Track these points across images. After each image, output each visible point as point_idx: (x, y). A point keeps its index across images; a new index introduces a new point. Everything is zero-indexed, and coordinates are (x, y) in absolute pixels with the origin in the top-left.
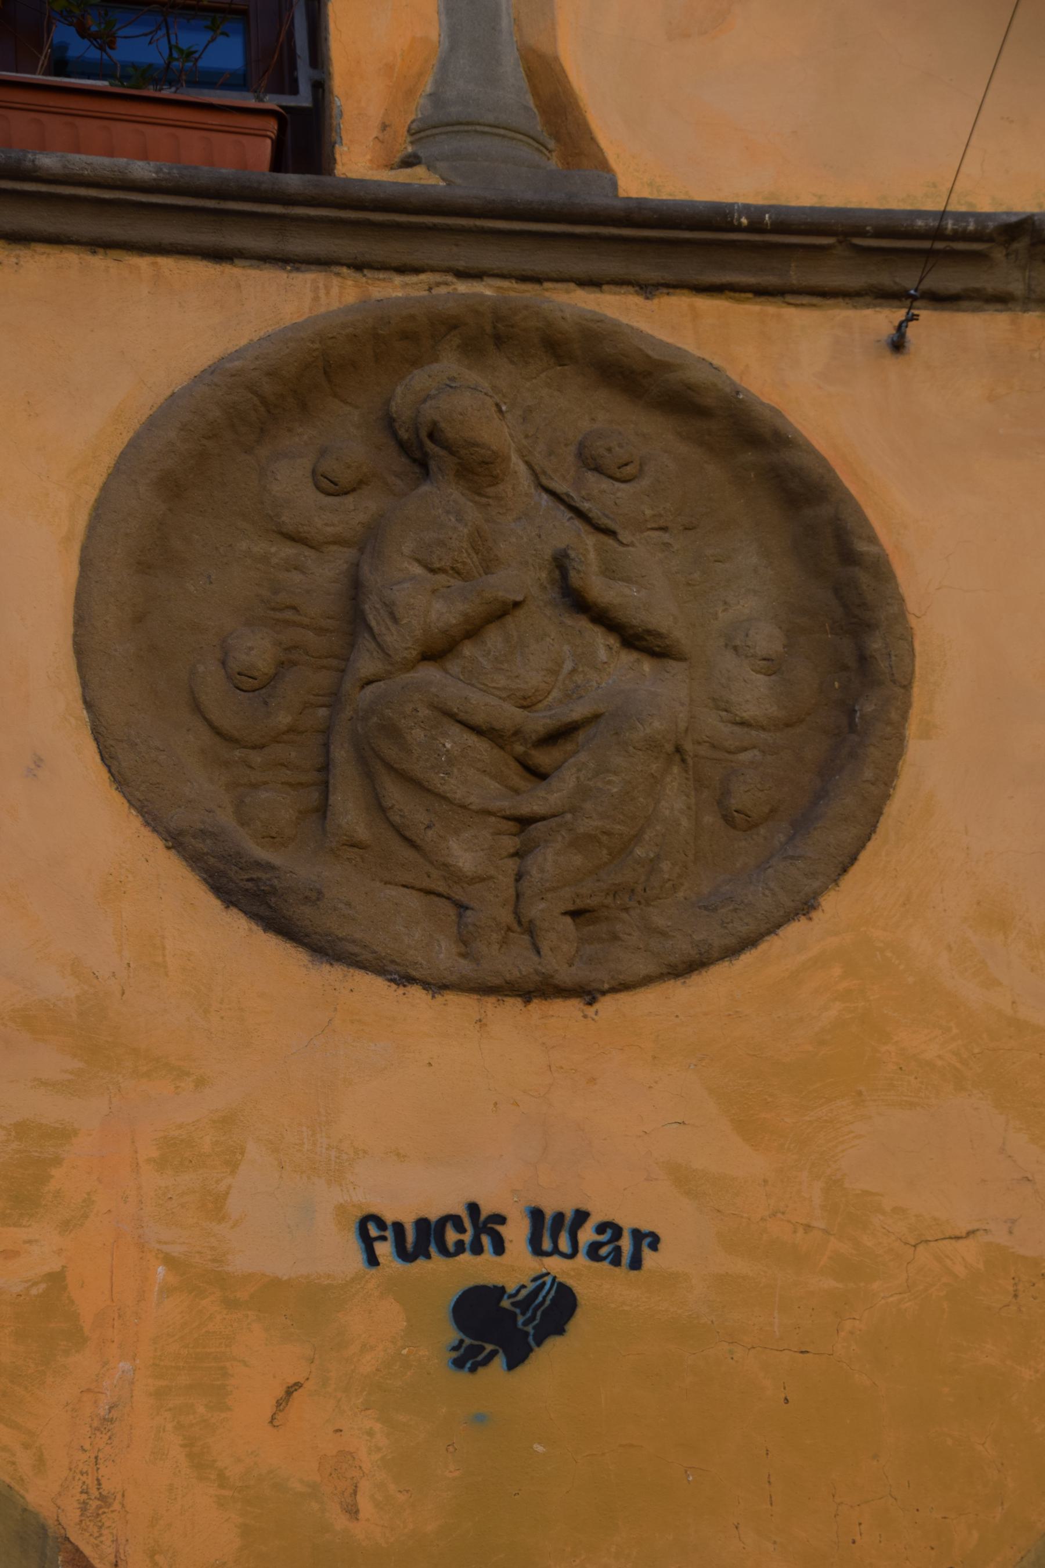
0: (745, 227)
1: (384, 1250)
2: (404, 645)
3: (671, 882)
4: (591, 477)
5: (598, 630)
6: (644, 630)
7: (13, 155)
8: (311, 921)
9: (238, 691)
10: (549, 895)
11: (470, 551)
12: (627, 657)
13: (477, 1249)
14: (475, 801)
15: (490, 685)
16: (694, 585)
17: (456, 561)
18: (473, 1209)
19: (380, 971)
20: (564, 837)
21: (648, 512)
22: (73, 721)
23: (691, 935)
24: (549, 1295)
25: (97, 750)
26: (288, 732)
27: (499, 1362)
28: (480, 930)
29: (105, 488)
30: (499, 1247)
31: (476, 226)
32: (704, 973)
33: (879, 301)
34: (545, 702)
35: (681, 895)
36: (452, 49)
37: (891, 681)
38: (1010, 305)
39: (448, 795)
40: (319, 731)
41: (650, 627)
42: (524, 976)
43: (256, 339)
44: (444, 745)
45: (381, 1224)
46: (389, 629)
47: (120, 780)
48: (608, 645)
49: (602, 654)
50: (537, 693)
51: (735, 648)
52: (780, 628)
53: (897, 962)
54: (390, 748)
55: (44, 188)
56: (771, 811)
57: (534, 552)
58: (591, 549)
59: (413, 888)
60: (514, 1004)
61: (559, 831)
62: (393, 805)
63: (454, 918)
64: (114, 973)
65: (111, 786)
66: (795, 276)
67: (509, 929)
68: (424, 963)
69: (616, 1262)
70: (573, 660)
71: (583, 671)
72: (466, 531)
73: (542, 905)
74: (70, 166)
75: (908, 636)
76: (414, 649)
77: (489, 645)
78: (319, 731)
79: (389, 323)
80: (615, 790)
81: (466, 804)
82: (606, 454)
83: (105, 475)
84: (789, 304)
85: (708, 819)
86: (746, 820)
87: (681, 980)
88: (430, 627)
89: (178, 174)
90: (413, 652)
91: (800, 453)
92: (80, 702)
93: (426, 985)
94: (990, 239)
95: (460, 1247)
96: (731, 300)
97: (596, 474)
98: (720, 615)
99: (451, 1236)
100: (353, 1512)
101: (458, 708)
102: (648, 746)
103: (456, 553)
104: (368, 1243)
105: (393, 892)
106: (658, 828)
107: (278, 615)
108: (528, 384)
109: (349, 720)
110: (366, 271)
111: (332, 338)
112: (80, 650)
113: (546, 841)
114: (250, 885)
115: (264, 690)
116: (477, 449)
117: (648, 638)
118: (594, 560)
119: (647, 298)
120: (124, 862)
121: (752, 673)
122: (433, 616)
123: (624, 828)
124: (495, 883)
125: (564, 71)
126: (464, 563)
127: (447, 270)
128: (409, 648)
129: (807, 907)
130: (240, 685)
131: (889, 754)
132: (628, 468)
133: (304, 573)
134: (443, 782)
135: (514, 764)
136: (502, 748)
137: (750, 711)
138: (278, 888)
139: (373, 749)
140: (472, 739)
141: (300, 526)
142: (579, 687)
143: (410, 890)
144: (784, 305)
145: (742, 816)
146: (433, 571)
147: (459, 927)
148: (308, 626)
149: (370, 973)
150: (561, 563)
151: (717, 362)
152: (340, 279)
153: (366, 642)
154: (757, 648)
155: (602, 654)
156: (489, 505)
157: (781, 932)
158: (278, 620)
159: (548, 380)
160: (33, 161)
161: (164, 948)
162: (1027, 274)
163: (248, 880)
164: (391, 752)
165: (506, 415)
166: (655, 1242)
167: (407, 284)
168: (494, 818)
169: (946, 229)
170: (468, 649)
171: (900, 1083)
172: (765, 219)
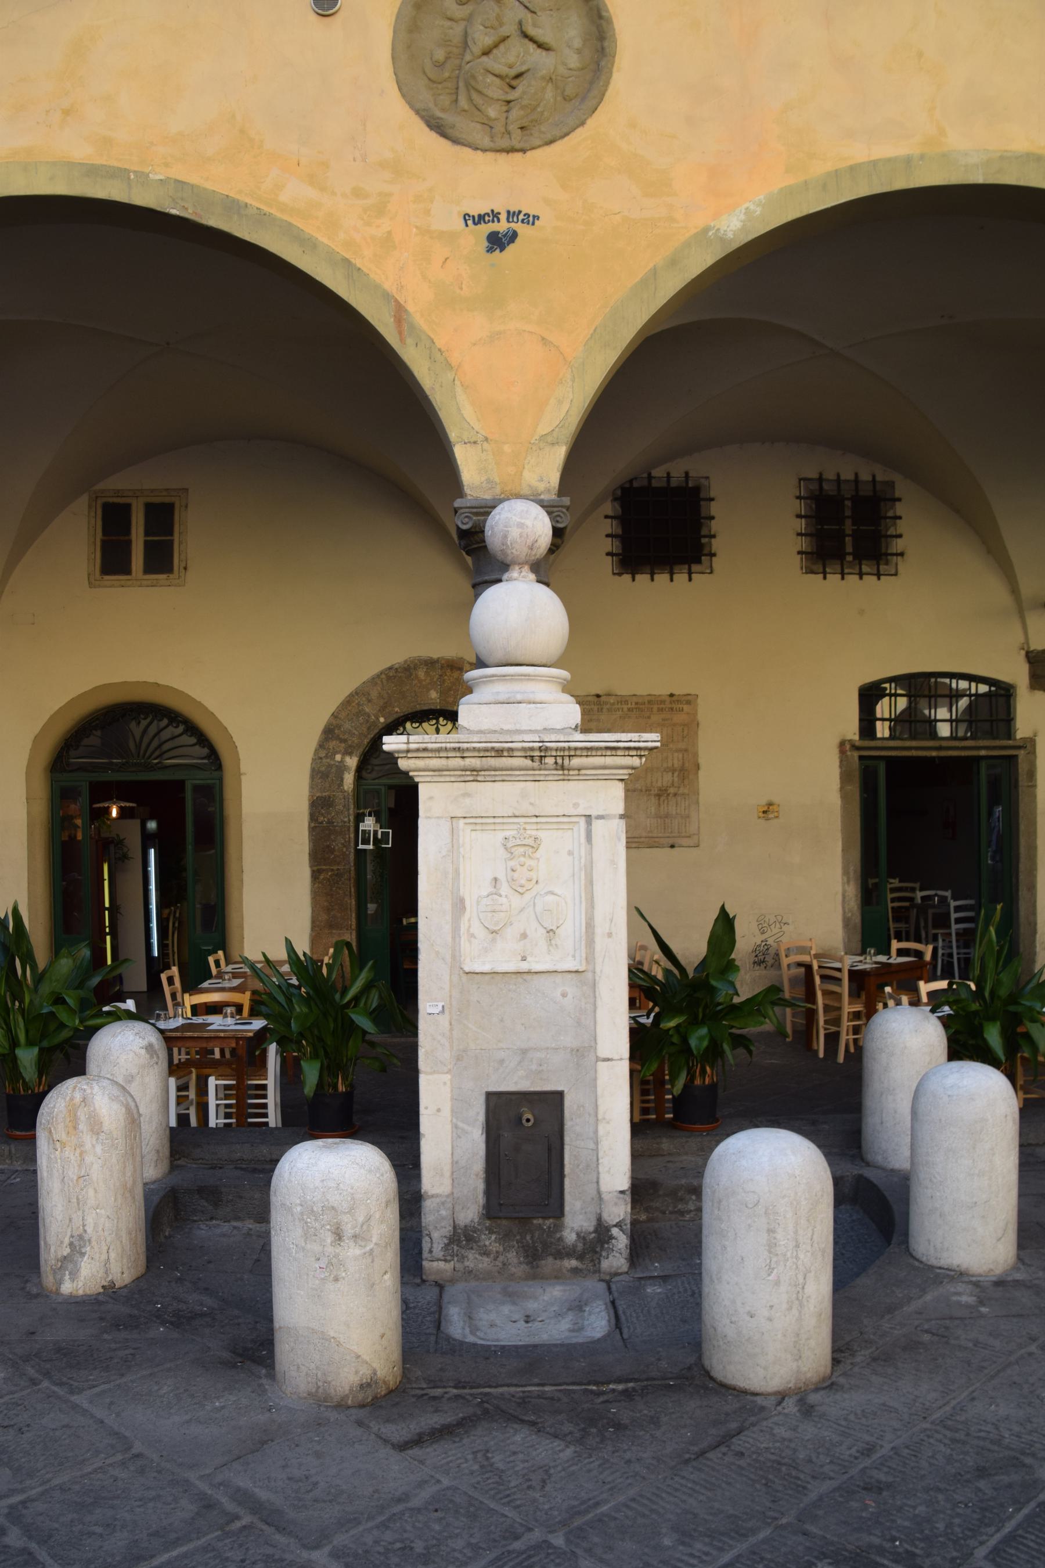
1: (470, 222)
12: (539, 51)
13: (493, 221)
14: (495, 96)
18: (492, 211)
19: (470, 147)
21: (547, 5)
24: (510, 233)
27: (498, 251)
29: (400, 9)
30: (499, 221)
40: (454, 1221)
45: (469, 216)
47: (403, 96)
49: (532, 50)
60: (504, 155)
69: (528, 224)
75: (615, 42)
78: (454, 1221)
85: (559, 98)
95: (489, 221)
99: (487, 218)
100: (461, 289)
104: (466, 221)
105: (473, 124)
112: (393, 58)
129: (583, 123)
137: (572, 66)
140: (495, 78)
146: (486, 27)
150: (520, 23)
153: (468, 51)
155: (532, 50)
164: (473, 83)
166: (538, 218)
170: (495, 51)
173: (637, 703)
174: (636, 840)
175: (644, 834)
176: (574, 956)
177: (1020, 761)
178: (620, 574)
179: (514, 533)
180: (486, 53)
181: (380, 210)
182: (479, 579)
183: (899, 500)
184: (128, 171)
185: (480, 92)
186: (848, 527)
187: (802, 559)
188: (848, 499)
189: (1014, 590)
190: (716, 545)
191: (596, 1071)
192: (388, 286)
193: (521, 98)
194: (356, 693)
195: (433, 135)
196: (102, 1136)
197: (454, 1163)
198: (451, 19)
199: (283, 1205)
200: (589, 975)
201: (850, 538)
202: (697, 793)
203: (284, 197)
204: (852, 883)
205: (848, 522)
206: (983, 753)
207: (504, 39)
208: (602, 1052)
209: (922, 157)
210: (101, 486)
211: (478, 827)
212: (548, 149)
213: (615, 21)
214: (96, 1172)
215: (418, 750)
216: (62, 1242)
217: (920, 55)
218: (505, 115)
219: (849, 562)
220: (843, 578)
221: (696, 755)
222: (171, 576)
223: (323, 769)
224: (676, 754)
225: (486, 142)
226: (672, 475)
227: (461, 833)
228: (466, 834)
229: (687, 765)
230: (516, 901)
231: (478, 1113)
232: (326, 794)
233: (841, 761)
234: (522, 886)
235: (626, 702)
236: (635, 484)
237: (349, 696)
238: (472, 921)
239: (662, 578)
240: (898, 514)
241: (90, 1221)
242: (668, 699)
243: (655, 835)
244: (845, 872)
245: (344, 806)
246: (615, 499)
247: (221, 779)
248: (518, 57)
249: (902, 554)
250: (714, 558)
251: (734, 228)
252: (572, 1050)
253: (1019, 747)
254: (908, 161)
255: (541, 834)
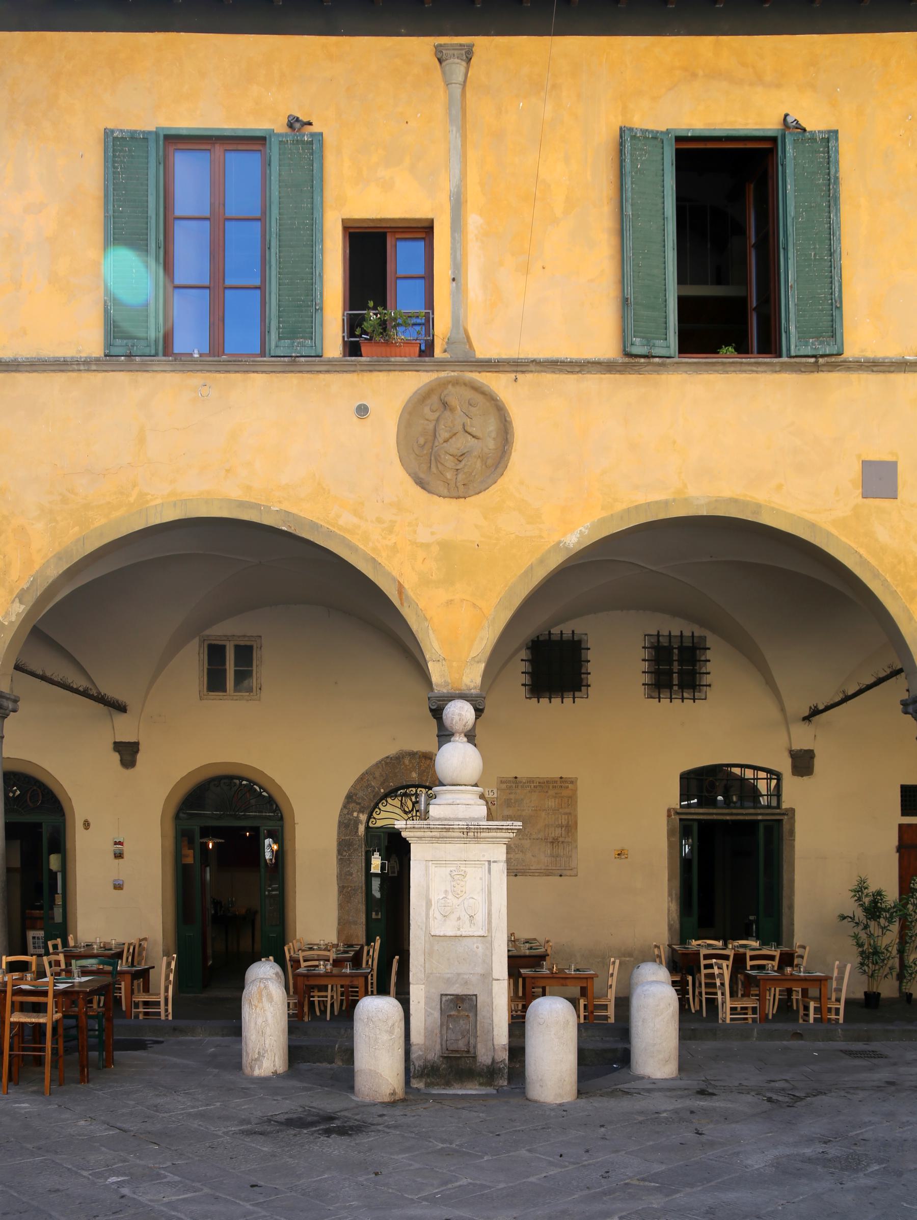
12: (473, 439)
60: (455, 499)
85: (484, 467)
100: (432, 575)
137: (490, 448)
164: (439, 459)
170: (450, 440)
173: (539, 783)
174: (538, 871)
175: (543, 868)
176: (482, 929)
177: (784, 823)
178: (530, 698)
179: (456, 718)
180: (446, 441)
181: (390, 530)
182: (442, 733)
183: (709, 649)
184: (261, 505)
185: (443, 465)
186: (676, 667)
187: (645, 688)
188: (675, 648)
189: (783, 710)
190: (591, 679)
191: (492, 985)
192: (395, 573)
194: (366, 773)
196: (273, 1003)
197: (426, 1029)
198: (427, 420)
199: (360, 1019)
200: (489, 938)
201: (677, 674)
202: (576, 841)
203: (341, 522)
204: (674, 902)
205: (676, 664)
206: (760, 817)
208: (495, 976)
209: (674, 500)
210: (208, 632)
211: (438, 865)
212: (477, 496)
214: (270, 1020)
215: (411, 828)
216: (254, 1052)
217: (674, 442)
219: (675, 690)
220: (671, 702)
221: (576, 816)
222: (252, 694)
223: (346, 821)
224: (563, 816)
225: (446, 492)
226: (563, 632)
227: (430, 868)
228: (432, 869)
229: (570, 823)
230: (455, 901)
231: (437, 1005)
232: (348, 837)
233: (668, 822)
234: (458, 894)
235: (533, 782)
236: (541, 638)
237: (362, 775)
238: (435, 912)
239: (556, 701)
240: (708, 659)
241: (267, 1042)
242: (559, 780)
243: (550, 868)
244: (670, 894)
245: (359, 846)
246: (528, 648)
247: (282, 827)
249: (709, 686)
250: (589, 688)
251: (573, 542)
252: (481, 975)
253: (784, 814)
254: (666, 503)
255: (467, 869)
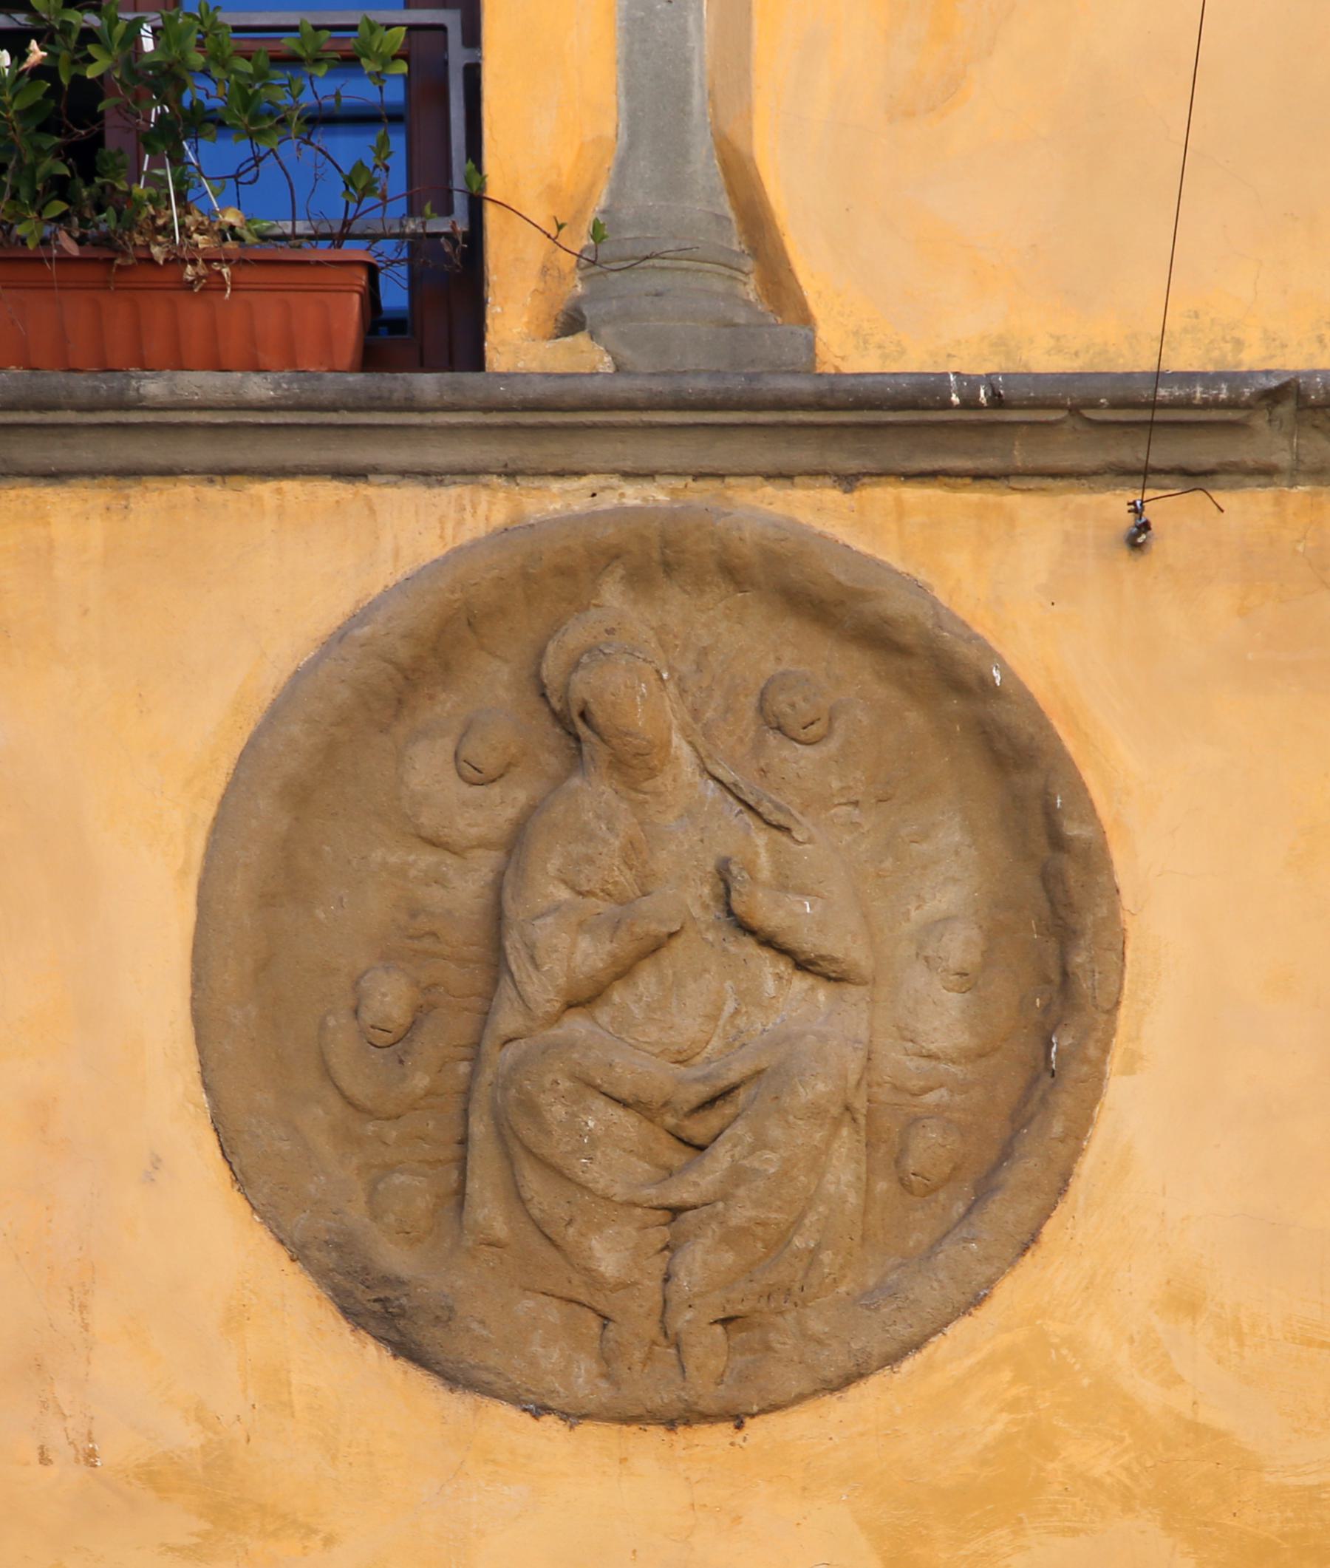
0: (957, 405)
2: (546, 997)
3: (833, 1276)
4: (772, 739)
5: (767, 955)
6: (816, 956)
7: (115, 384)
8: (441, 1347)
9: (372, 1047)
10: (697, 1302)
11: (622, 867)
12: (801, 983)
15: (641, 1039)
16: (885, 877)
17: (607, 881)
19: (515, 1400)
20: (714, 1231)
21: (836, 784)
22: (191, 1108)
23: (849, 1343)
25: (217, 1144)
26: (426, 1096)
28: (621, 1348)
29: (223, 802)
31: (642, 421)
32: (862, 1384)
33: (1121, 479)
34: (704, 1055)
35: (842, 1289)
36: (631, 146)
37: (1094, 1005)
38: (1275, 479)
39: (590, 1185)
41: (823, 952)
42: (666, 1404)
43: (391, 585)
44: (587, 1123)
46: (529, 976)
47: (241, 1180)
48: (777, 974)
49: (770, 986)
50: (693, 1046)
51: (927, 959)
52: (980, 927)
53: (1074, 1360)
54: (529, 1129)
55: (151, 417)
56: (954, 1169)
57: (695, 863)
58: (762, 851)
59: (553, 1296)
60: (656, 1434)
61: (709, 1224)
62: (533, 1197)
63: (596, 1330)
64: (238, 1416)
65: (233, 1187)
66: (1019, 458)
67: (654, 1343)
68: (561, 1390)
70: (736, 1000)
71: (746, 1012)
72: (617, 843)
73: (689, 1315)
74: (178, 392)
76: (557, 1001)
77: (641, 988)
79: (541, 559)
80: (772, 1170)
81: (610, 1196)
82: (788, 710)
83: (224, 785)
84: (1014, 489)
85: (881, 1186)
86: (925, 1184)
87: (838, 1394)
88: (574, 972)
89: (299, 389)
90: (555, 1003)
91: (1009, 706)
92: (199, 1083)
93: (565, 1416)
94: (1248, 406)
96: (945, 488)
97: (779, 735)
98: (913, 914)
101: (602, 1079)
102: (809, 1115)
103: (606, 873)
106: (821, 1209)
107: (416, 945)
108: (704, 618)
109: (490, 1085)
110: (519, 479)
111: (475, 584)
112: (199, 1018)
113: (696, 1236)
114: (377, 1306)
115: (400, 1045)
116: (630, 739)
117: (821, 963)
118: (765, 864)
119: (845, 492)
120: (248, 1281)
121: (945, 991)
122: (578, 957)
123: (781, 1216)
124: (639, 1289)
125: (759, 178)
126: (616, 883)
127: (613, 472)
128: (552, 1000)
130: (373, 1041)
131: (1083, 1101)
132: (813, 728)
133: (444, 887)
134: (585, 1169)
135: (664, 1137)
136: (651, 1121)
137: (938, 1043)
138: (407, 1308)
139: (511, 1128)
140: (617, 1113)
141: (440, 829)
142: (742, 1032)
143: (551, 1298)
144: (1009, 491)
145: (920, 1178)
147: (601, 1341)
148: (448, 956)
149: (505, 1403)
150: (723, 875)
151: (922, 577)
152: (488, 492)
154: (950, 961)
155: (770, 986)
156: (647, 802)
157: (948, 1331)
158: (416, 951)
159: (728, 611)
160: (138, 389)
161: (289, 1384)
162: (1295, 440)
163: (375, 1301)
164: (529, 1133)
165: (667, 684)
167: (567, 491)
168: (640, 1210)
169: (1194, 398)
170: (618, 995)
171: (1064, 1506)
172: (979, 396)
193: (725, 1197)
195: (373, 1355)
198: (434, 843)
207: (655, 947)
212: (837, 1408)
213: (1118, 856)
218: (657, 1265)
248: (713, 1018)
